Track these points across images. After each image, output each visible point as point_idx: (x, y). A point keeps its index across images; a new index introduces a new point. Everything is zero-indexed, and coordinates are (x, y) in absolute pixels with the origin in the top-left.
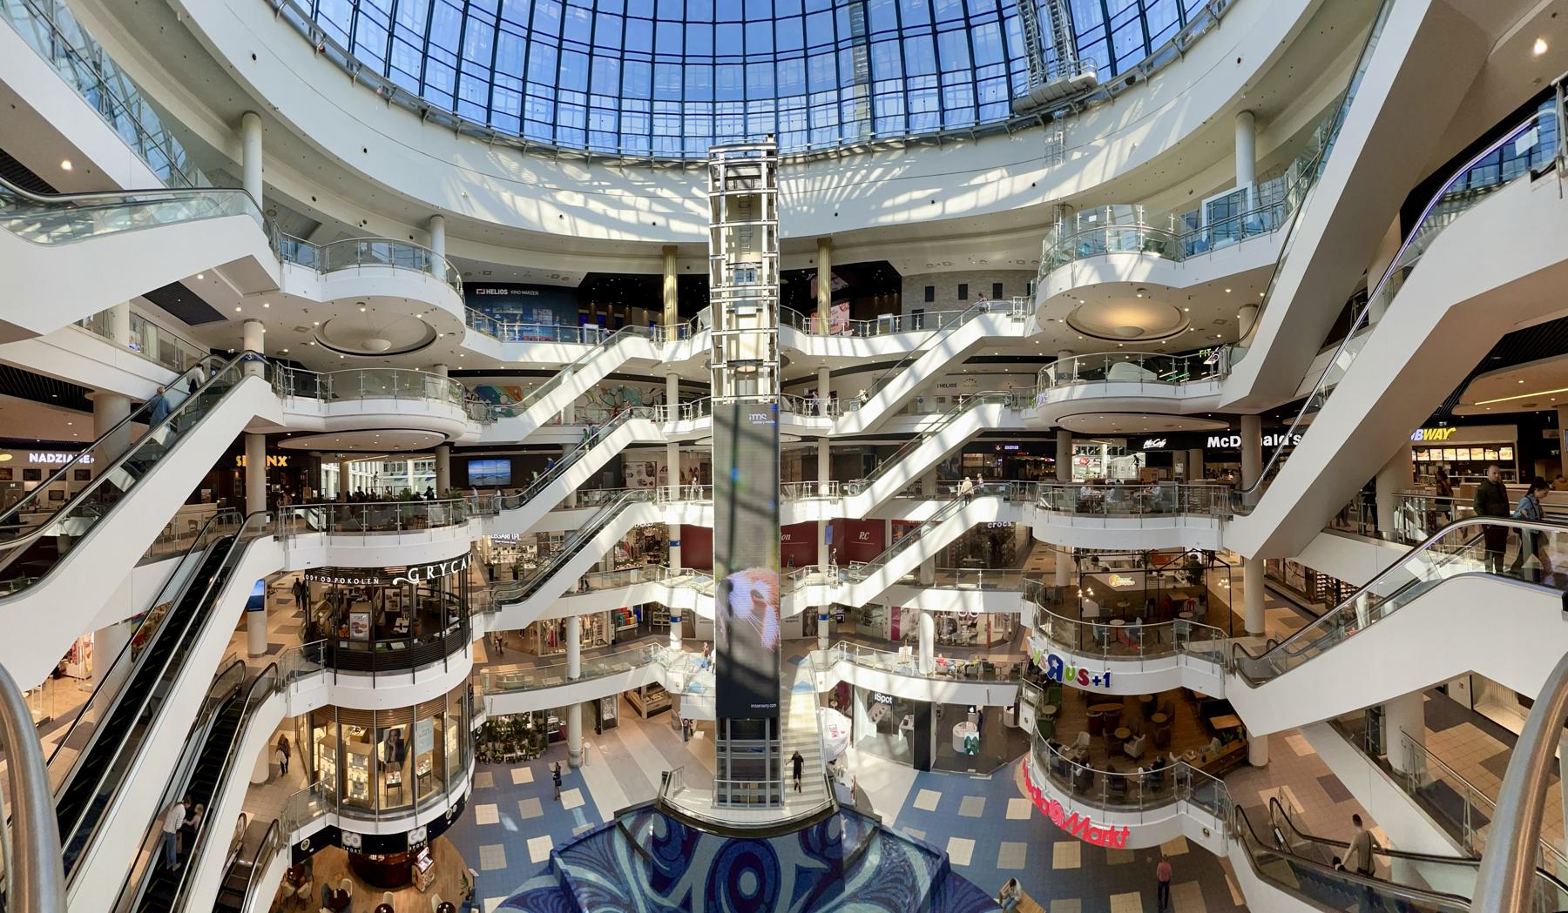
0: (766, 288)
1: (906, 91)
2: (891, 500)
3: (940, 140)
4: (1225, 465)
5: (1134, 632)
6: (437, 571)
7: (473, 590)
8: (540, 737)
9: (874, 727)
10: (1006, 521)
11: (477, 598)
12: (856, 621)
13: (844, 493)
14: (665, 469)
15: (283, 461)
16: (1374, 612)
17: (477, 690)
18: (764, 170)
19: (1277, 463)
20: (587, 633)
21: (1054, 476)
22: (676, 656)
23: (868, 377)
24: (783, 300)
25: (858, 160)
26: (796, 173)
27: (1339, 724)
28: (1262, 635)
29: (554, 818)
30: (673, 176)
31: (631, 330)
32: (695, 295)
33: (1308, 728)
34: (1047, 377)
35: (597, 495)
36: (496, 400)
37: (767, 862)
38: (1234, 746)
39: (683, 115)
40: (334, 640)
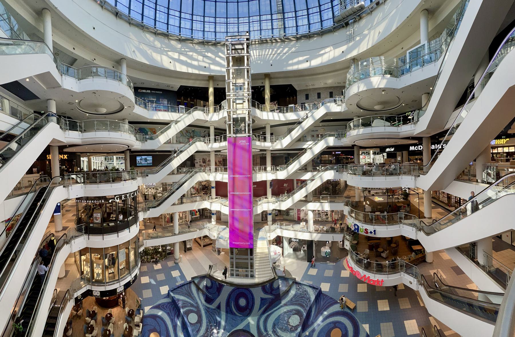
0: (246, 93)
1: (296, 17)
2: (296, 172)
3: (308, 36)
4: (416, 157)
5: (384, 216)
6: (126, 197)
7: (139, 203)
8: (164, 254)
9: (292, 250)
10: (337, 179)
11: (141, 206)
13: (278, 170)
14: (209, 161)
15: (66, 157)
16: (475, 208)
17: (141, 239)
19: (437, 156)
20: (181, 218)
21: (354, 162)
22: (214, 226)
23: (285, 128)
24: (253, 98)
25: (279, 44)
26: (256, 47)
27: (460, 249)
28: (431, 218)
29: (169, 280)
30: (212, 48)
31: (196, 108)
32: (220, 95)
33: (449, 250)
34: (350, 127)
35: (184, 170)
36: (146, 134)
37: (249, 296)
38: (420, 256)
39: (215, 23)
40: (88, 223)
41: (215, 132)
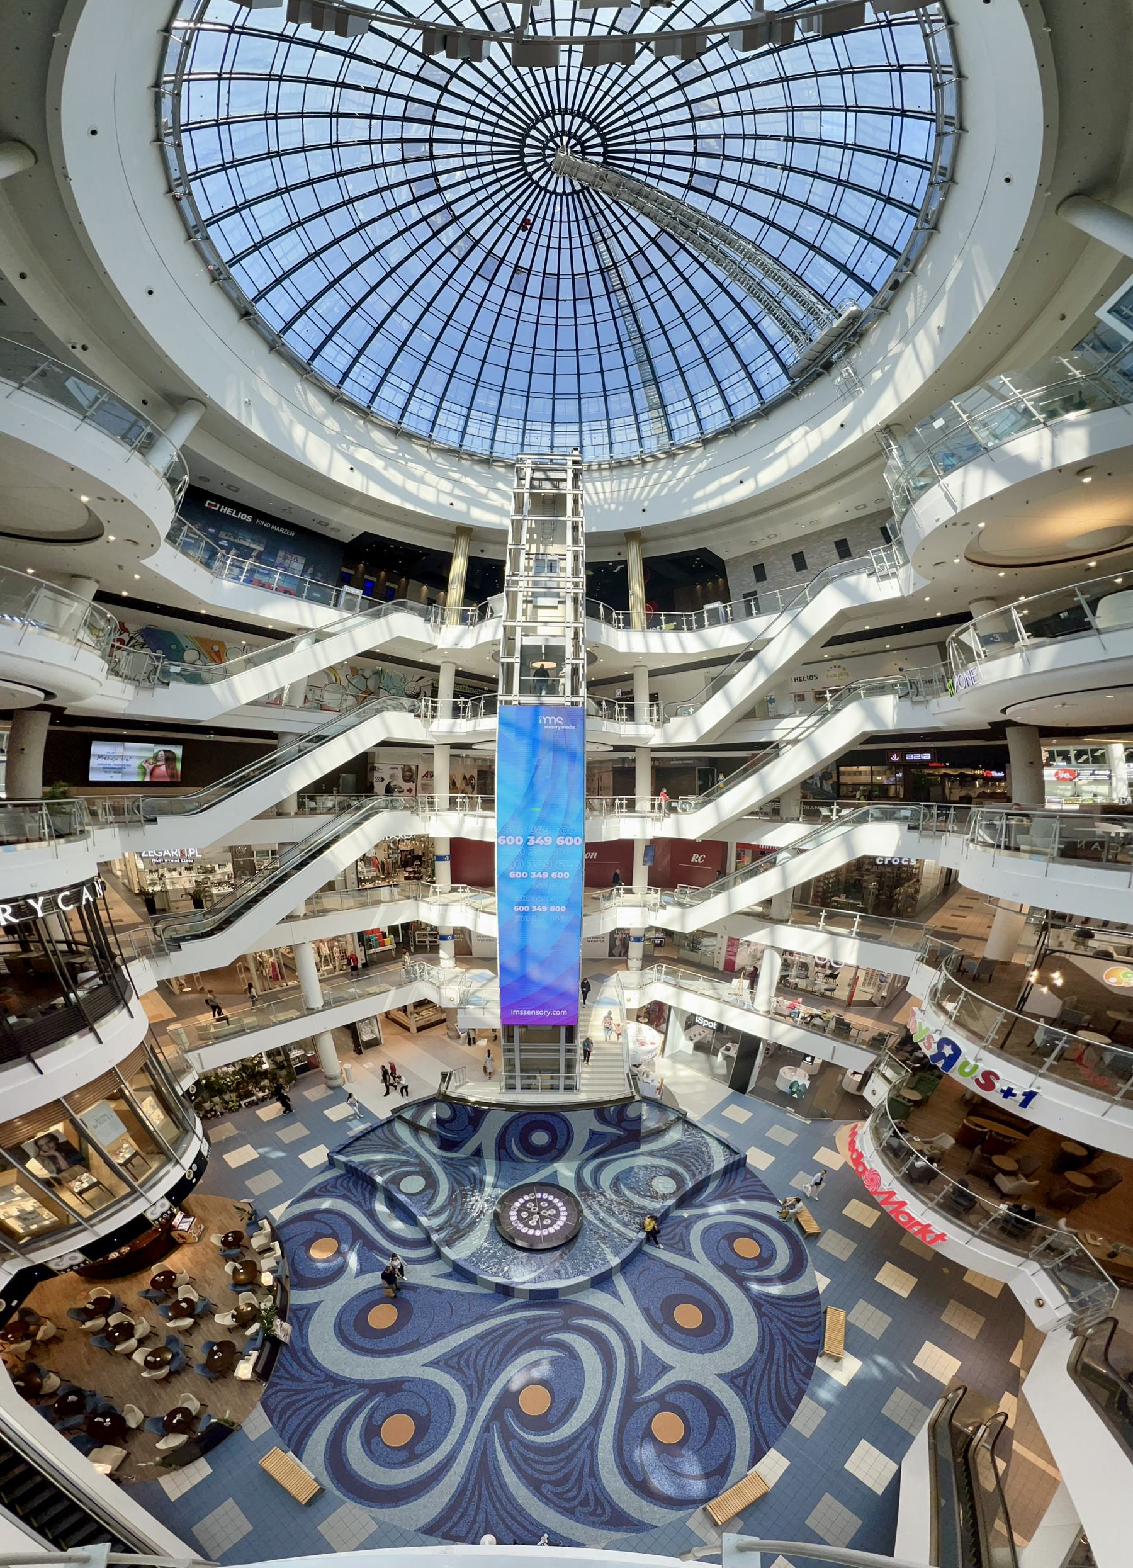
0: (570, 580)
2: (738, 819)
3: (734, 428)
9: (691, 1045)
11: (123, 944)
12: (679, 946)
14: (429, 775)
18: (570, 475)
24: (590, 593)
25: (662, 463)
31: (403, 605)
32: (486, 580)
35: (329, 801)
36: (176, 655)
37: (559, 1127)
41: (457, 684)
